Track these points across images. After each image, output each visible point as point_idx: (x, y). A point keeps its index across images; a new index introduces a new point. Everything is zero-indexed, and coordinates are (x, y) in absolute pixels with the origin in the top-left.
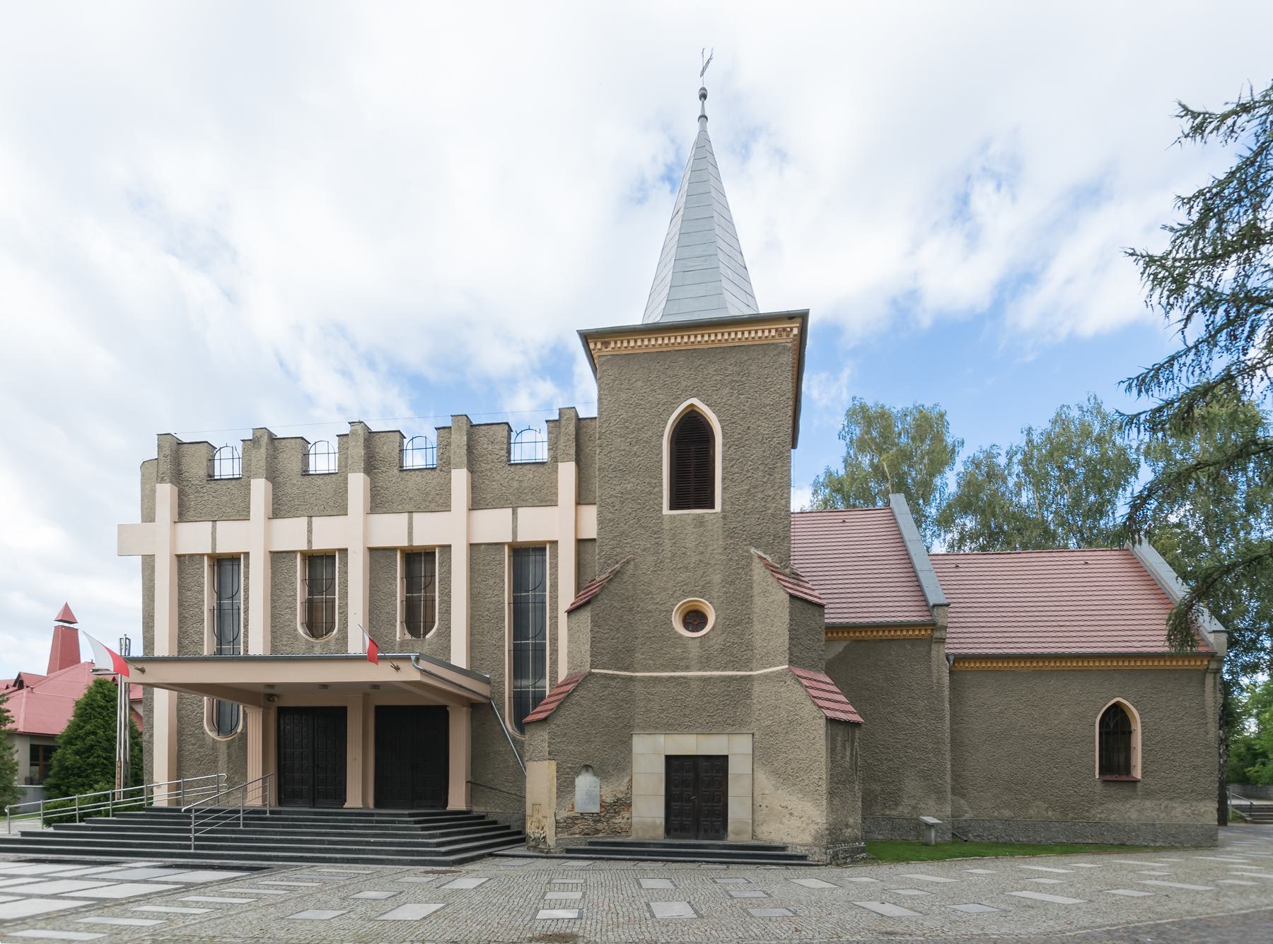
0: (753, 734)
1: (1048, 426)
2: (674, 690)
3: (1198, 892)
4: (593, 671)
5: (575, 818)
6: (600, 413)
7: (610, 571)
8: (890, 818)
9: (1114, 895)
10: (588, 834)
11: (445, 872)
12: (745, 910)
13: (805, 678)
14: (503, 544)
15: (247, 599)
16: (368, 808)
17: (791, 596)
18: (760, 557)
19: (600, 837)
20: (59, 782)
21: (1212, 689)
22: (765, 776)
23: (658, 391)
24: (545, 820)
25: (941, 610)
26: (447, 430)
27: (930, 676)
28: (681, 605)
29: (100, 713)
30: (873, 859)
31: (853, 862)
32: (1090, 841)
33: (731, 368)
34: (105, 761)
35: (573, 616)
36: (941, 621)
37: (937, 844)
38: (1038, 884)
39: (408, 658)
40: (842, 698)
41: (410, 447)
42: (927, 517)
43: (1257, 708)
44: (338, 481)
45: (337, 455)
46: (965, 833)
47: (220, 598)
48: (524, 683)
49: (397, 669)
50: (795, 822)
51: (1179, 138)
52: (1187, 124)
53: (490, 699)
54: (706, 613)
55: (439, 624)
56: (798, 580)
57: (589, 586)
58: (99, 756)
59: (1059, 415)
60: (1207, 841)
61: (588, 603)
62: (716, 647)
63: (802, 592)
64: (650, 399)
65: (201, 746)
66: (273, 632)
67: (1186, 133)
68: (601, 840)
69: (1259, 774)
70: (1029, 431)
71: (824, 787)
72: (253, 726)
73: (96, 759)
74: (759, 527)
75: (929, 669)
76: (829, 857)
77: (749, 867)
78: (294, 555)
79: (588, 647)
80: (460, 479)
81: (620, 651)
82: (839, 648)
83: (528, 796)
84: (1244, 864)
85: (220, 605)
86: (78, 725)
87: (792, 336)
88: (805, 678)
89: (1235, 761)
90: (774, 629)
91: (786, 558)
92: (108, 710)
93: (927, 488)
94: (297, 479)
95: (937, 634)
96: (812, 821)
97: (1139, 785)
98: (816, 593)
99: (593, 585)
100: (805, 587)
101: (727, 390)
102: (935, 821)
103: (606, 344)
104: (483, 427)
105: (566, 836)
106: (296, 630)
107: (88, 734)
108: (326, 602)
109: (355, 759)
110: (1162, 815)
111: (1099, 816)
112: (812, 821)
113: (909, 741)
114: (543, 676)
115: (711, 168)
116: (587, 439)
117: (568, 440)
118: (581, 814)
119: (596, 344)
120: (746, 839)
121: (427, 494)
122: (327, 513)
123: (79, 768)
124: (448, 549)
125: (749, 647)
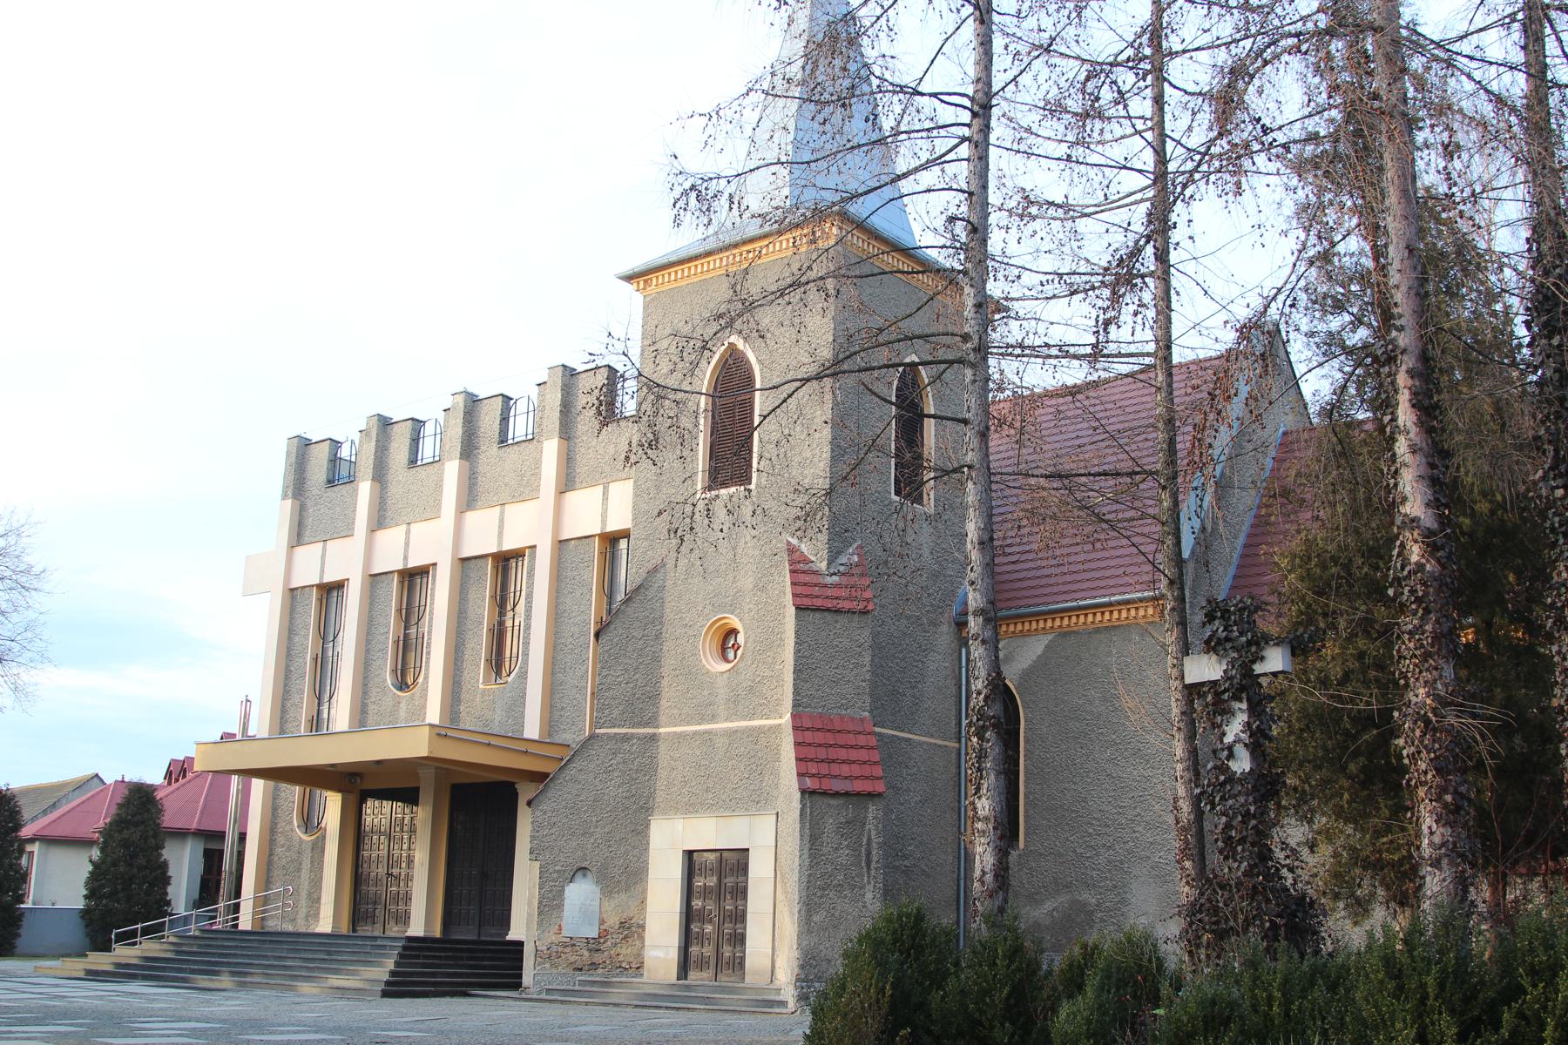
4: (598, 731)
65: (289, 849)
81: (638, 699)
113: (1138, 810)
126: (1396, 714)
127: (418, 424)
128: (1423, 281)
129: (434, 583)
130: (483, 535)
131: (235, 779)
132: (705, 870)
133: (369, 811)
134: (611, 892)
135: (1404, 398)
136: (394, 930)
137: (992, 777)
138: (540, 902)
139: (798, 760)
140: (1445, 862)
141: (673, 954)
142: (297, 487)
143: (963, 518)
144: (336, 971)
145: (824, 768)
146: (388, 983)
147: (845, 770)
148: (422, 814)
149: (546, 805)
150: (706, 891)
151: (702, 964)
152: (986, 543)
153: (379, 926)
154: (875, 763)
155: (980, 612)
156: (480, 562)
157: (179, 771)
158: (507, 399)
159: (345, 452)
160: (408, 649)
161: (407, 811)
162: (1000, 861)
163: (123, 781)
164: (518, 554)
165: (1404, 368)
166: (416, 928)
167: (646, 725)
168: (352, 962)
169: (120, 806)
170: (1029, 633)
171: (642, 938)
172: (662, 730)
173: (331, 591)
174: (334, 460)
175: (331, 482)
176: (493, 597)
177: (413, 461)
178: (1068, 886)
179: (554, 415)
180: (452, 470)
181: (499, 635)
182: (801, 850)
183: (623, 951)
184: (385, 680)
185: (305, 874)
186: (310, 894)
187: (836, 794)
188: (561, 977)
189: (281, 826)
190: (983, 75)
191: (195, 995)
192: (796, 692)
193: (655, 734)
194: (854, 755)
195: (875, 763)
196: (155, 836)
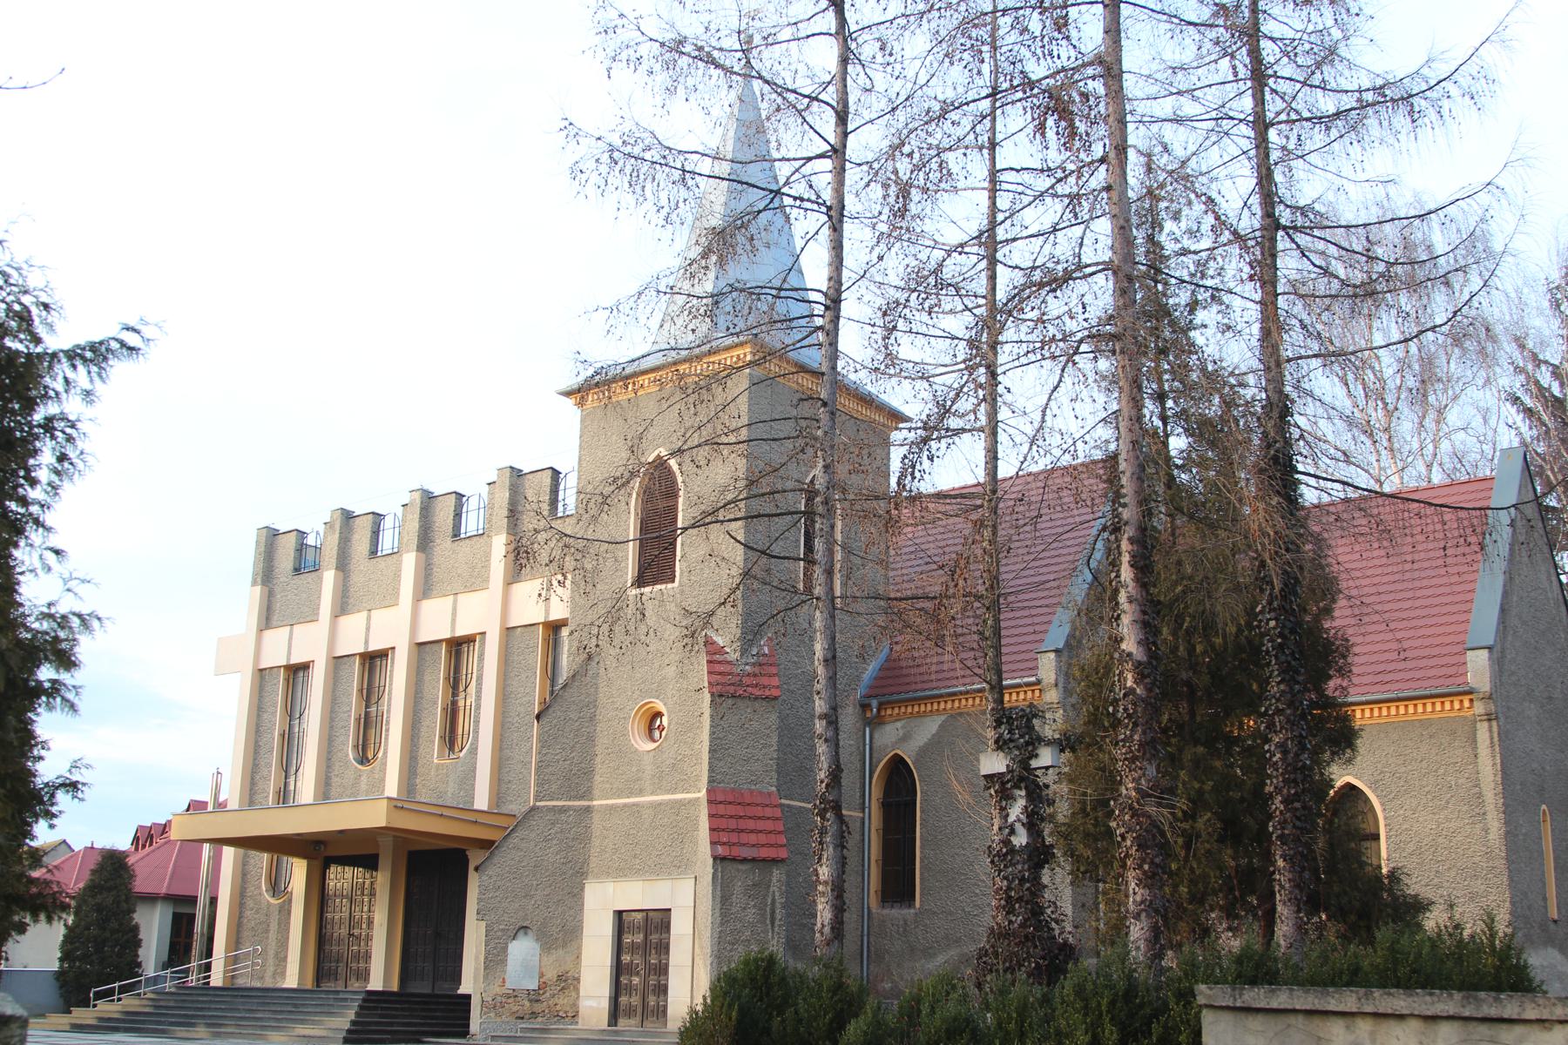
21: (1489, 750)
65: (257, 912)
85: (367, 714)
126: (1112, 803)
127: (378, 518)
128: (1142, 468)
129: (392, 666)
130: (438, 622)
131: (206, 846)
132: (633, 929)
133: (332, 876)
134: (549, 949)
135: (1126, 558)
136: (355, 985)
137: (831, 849)
138: (486, 958)
139: (712, 830)
140: (1143, 915)
141: (605, 1004)
142: (266, 574)
143: (812, 639)
144: (302, 1022)
145: (734, 838)
146: (349, 1031)
147: (753, 838)
148: (382, 879)
149: (492, 870)
150: (633, 948)
151: (630, 1012)
152: (831, 660)
153: (341, 983)
154: (780, 833)
155: (823, 717)
156: (435, 647)
157: (147, 837)
158: (460, 496)
159: (311, 541)
160: (369, 725)
161: (367, 875)
162: (836, 916)
163: (92, 848)
164: (469, 640)
165: (1126, 536)
166: (376, 983)
167: (582, 798)
168: (316, 1013)
169: (93, 872)
170: (920, 715)
171: (577, 990)
172: (595, 803)
173: (297, 671)
174: (301, 548)
175: (297, 570)
176: (447, 679)
177: (373, 552)
178: (958, 941)
179: (502, 512)
180: (410, 560)
181: (452, 713)
182: (713, 909)
183: (561, 1002)
184: (347, 755)
185: (273, 935)
186: (277, 954)
187: (744, 860)
188: (506, 1024)
189: (251, 890)
190: (835, 275)
191: (175, 1042)
192: (711, 769)
193: (589, 807)
194: (761, 825)
195: (780, 833)
196: (127, 900)
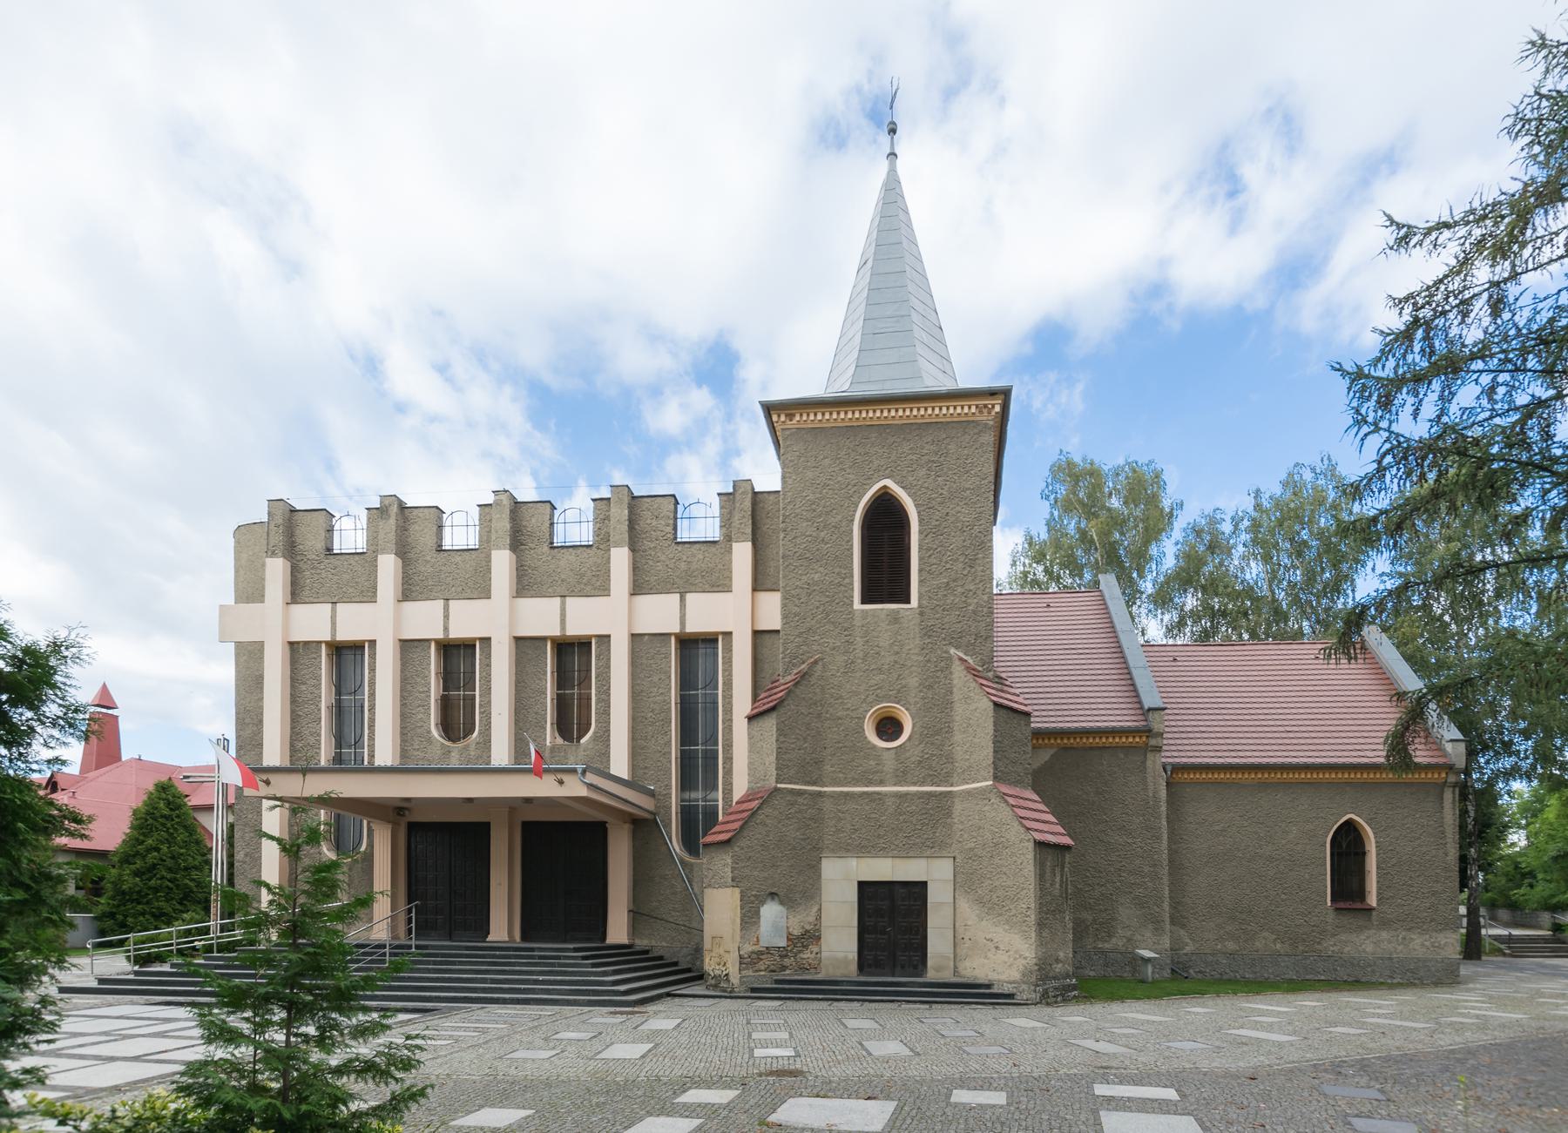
0: (954, 858)
1: (1277, 490)
2: (867, 808)
3: (1415, 1030)
4: (779, 786)
5: (761, 953)
6: (783, 488)
7: (795, 671)
8: (1103, 952)
9: (1330, 1032)
10: (774, 971)
11: (633, 1013)
12: (960, 1048)
13: (1011, 796)
14: (669, 635)
15: (372, 695)
16: (515, 942)
17: (996, 704)
18: (961, 659)
19: (788, 974)
20: (114, 910)
21: (1451, 806)
22: (967, 905)
23: (848, 471)
24: (727, 955)
25: (1156, 715)
26: (605, 502)
27: (1145, 789)
28: (874, 713)
29: (163, 825)
30: (1085, 997)
31: (1064, 1000)
32: (1323, 978)
33: (927, 447)
34: (169, 884)
35: (754, 723)
36: (1157, 727)
37: (1154, 982)
38: (1256, 1022)
39: (574, 771)
40: (1042, 807)
41: (561, 520)
42: (1142, 593)
43: (1526, 818)
44: (478, 559)
45: (478, 528)
46: (1186, 969)
47: (339, 693)
48: (693, 795)
49: (561, 782)
50: (1001, 957)
51: (1297, 465)
52: (1390, 235)
53: (654, 814)
54: (893, 715)
55: (596, 726)
56: (1002, 684)
57: (772, 689)
58: (163, 878)
59: (1290, 475)
60: (1446, 978)
61: (773, 709)
62: (913, 759)
63: (1006, 699)
64: (840, 479)
66: (402, 734)
67: (1391, 244)
68: (788, 978)
69: (1526, 897)
70: (1258, 493)
71: (1032, 918)
72: (381, 847)
73: (159, 882)
74: (959, 625)
75: (1144, 781)
76: (1038, 995)
77: (953, 1006)
78: (427, 644)
79: (773, 758)
80: (620, 559)
82: (1045, 756)
83: (706, 928)
84: (1477, 1001)
85: (339, 702)
86: (137, 840)
87: (993, 413)
88: (1011, 796)
89: (1503, 882)
90: (976, 740)
91: (988, 661)
92: (173, 820)
93: (1141, 558)
94: (431, 556)
95: (1153, 742)
96: (1020, 956)
97: (1374, 913)
98: (1020, 699)
99: (777, 687)
100: (1009, 693)
101: (923, 472)
102: (1152, 955)
103: (791, 416)
104: (645, 499)
105: (750, 973)
106: (429, 732)
107: (149, 850)
108: (464, 700)
109: (500, 884)
110: (1400, 948)
111: (1331, 948)
112: (1020, 956)
114: (715, 787)
115: (902, 215)
116: (764, 516)
117: (744, 517)
118: (767, 948)
119: (779, 416)
120: (947, 976)
121: (582, 576)
122: (466, 595)
123: (139, 892)
124: (606, 640)
125: (950, 759)
